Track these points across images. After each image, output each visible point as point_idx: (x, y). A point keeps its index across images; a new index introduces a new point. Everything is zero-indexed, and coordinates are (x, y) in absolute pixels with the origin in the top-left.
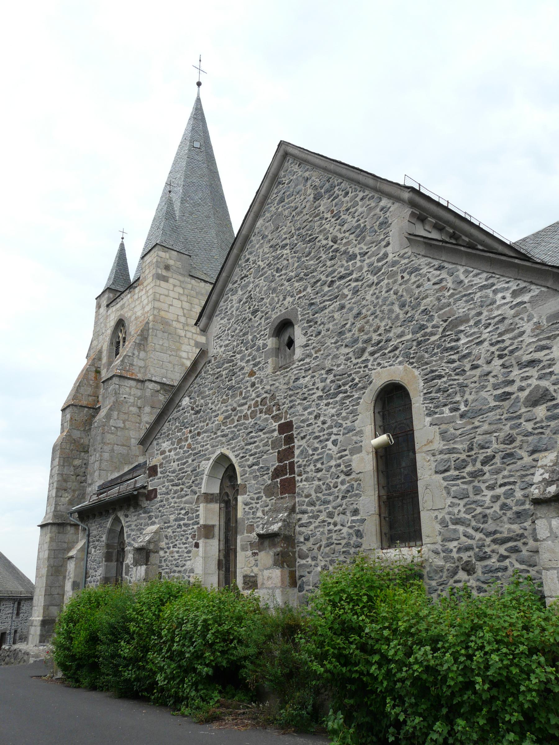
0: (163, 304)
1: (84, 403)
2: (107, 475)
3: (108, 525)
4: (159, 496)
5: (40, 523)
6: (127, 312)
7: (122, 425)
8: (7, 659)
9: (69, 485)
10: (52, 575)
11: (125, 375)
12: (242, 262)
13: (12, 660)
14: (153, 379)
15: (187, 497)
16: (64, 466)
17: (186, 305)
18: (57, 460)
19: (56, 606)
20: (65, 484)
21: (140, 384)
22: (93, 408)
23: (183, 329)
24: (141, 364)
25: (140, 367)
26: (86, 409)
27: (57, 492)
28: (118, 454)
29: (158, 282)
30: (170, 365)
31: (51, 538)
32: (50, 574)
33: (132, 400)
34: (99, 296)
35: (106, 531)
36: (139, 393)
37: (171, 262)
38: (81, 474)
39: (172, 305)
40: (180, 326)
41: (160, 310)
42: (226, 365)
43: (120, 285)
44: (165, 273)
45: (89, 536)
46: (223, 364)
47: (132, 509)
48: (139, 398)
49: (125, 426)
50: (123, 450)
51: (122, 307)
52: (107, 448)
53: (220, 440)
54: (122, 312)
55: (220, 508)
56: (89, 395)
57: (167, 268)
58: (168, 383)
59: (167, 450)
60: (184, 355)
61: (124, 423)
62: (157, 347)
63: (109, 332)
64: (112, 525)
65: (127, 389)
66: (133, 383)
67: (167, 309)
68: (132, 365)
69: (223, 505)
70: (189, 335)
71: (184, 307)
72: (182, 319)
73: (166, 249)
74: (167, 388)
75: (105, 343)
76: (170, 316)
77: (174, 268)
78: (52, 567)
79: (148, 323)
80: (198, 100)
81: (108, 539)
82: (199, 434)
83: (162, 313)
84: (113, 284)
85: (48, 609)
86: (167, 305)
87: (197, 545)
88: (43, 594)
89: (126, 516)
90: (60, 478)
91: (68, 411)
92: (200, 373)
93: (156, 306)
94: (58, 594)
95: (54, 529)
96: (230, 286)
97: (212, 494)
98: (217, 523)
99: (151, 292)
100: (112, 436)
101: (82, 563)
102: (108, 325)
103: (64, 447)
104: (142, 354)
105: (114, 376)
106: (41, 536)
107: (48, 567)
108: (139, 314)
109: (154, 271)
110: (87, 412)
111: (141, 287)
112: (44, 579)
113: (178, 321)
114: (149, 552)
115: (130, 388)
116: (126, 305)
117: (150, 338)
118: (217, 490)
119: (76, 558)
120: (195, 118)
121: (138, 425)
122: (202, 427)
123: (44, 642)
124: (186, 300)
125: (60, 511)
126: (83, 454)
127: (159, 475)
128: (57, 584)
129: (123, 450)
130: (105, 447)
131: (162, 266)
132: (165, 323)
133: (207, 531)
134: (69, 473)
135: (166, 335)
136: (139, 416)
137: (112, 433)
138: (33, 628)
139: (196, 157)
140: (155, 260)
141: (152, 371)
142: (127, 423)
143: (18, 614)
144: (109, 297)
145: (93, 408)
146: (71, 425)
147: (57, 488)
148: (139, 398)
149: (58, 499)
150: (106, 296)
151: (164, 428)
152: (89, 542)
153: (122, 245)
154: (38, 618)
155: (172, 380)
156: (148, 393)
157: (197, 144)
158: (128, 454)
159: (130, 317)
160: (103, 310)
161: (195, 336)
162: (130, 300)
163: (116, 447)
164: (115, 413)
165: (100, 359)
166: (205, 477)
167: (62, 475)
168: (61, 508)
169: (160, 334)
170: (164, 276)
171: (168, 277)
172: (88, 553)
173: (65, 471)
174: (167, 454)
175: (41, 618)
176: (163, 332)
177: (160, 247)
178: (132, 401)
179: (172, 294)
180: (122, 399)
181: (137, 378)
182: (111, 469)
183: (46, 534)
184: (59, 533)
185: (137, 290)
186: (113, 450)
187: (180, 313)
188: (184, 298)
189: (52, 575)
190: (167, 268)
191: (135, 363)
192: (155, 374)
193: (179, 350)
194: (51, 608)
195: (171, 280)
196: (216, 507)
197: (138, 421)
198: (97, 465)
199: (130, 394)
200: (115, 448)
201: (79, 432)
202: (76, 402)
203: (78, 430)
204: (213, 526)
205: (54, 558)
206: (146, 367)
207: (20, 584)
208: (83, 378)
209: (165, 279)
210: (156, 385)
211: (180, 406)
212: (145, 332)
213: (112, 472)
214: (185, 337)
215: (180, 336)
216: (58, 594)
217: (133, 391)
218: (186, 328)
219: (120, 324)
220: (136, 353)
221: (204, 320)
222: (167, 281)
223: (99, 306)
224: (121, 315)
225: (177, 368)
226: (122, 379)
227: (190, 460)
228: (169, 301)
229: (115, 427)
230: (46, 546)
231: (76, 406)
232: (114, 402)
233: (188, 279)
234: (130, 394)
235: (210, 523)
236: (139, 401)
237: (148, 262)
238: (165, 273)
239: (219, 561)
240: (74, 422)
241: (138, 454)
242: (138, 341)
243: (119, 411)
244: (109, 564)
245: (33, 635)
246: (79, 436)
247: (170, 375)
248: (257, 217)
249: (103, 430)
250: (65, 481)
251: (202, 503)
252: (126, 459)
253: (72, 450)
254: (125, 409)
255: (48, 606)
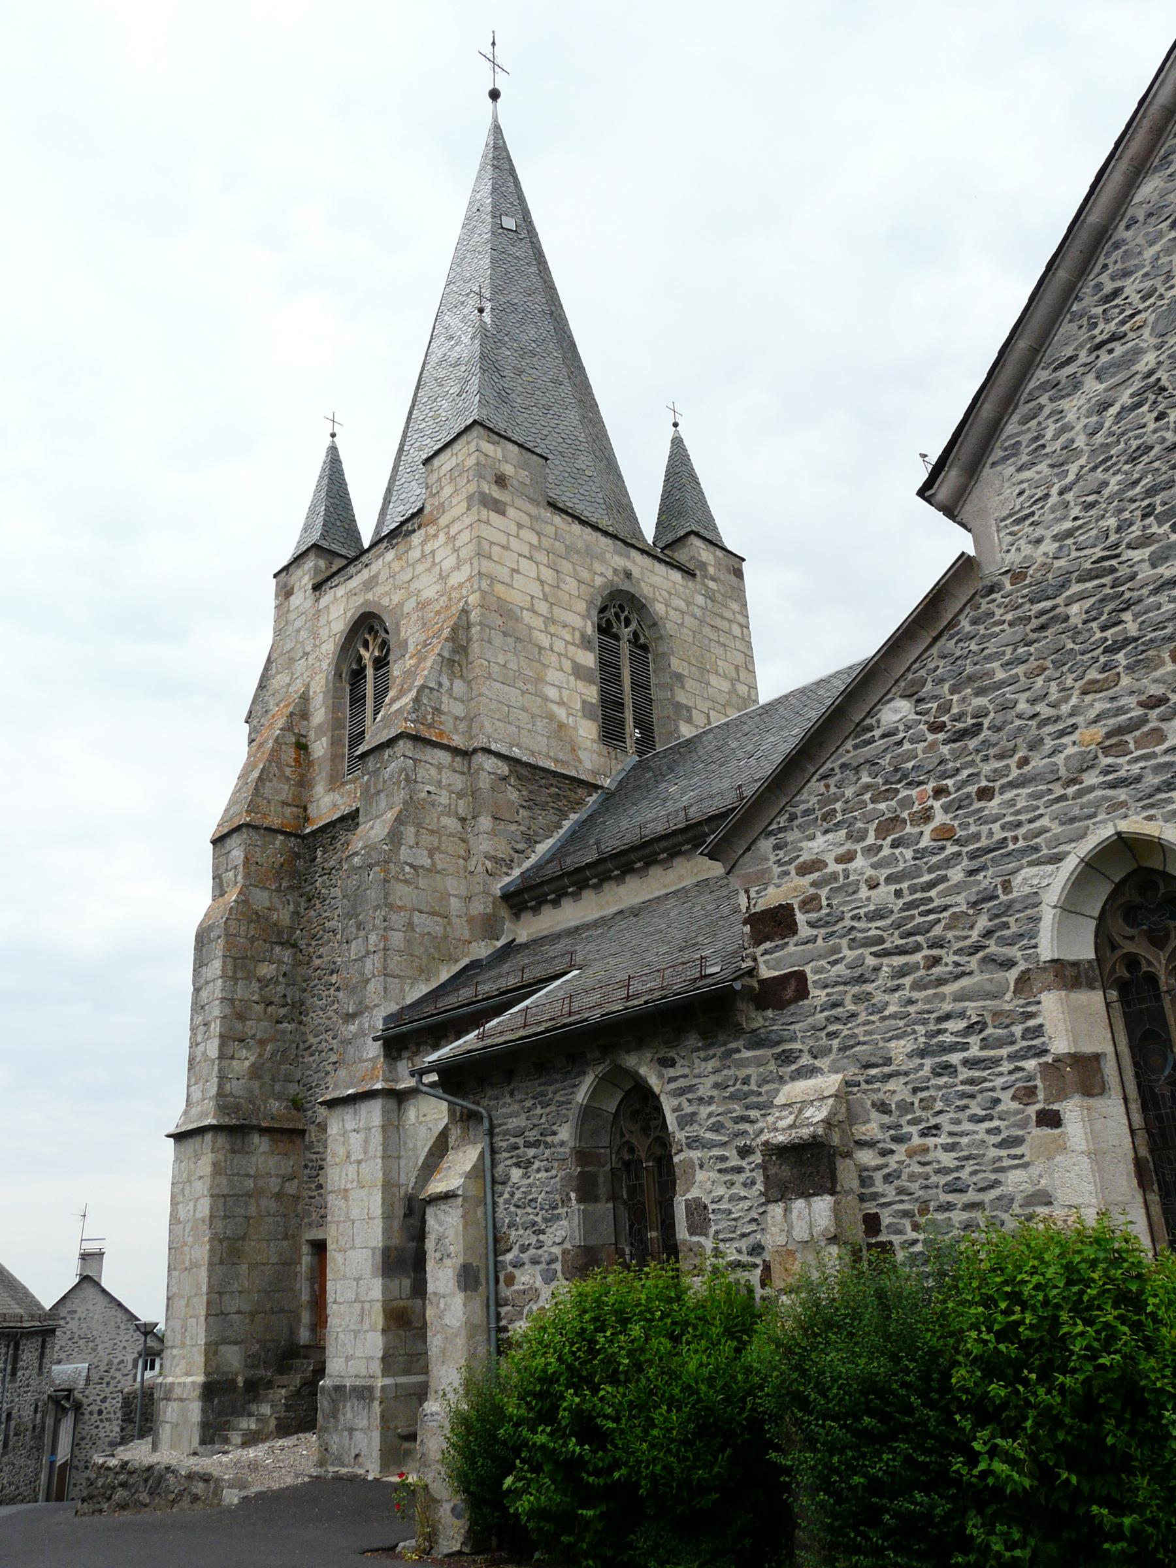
0: (499, 567)
1: (276, 822)
2: (402, 990)
3: (581, 1095)
4: (814, 992)
5: (172, 1129)
6: (387, 593)
7: (427, 862)
8: (120, 1494)
9: (251, 1027)
10: (221, 1262)
11: (427, 735)
12: (1088, 302)
13: (144, 1497)
14: (493, 747)
15: (964, 982)
16: (235, 979)
17: (548, 574)
18: (217, 964)
19: (236, 1343)
20: (239, 1026)
21: (458, 759)
22: (297, 836)
23: (546, 631)
24: (459, 710)
25: (457, 718)
26: (281, 838)
27: (222, 1047)
28: (423, 935)
29: (484, 512)
30: (524, 717)
31: (214, 1164)
32: (216, 1260)
33: (444, 799)
34: (286, 569)
35: (573, 1113)
36: (459, 782)
37: (508, 470)
38: (276, 1000)
39: (517, 571)
40: (538, 622)
41: (493, 580)
42: (1075, 588)
43: (333, 549)
44: (496, 492)
45: (491, 1133)
46: (1064, 586)
47: (693, 1041)
48: (460, 795)
49: (434, 864)
50: (433, 926)
51: (370, 584)
52: (398, 919)
53: (1105, 798)
54: (370, 596)
55: (1108, 1005)
56: (284, 804)
57: (501, 481)
58: (524, 759)
59: (830, 858)
60: (552, 693)
61: (431, 856)
62: (495, 669)
63: (329, 648)
64: (594, 1094)
65: (433, 771)
66: (443, 757)
67: (507, 580)
68: (437, 711)
69: (1114, 994)
70: (559, 646)
71: (543, 578)
72: (542, 607)
73: (496, 438)
74: (524, 772)
75: (317, 674)
76: (516, 598)
77: (516, 483)
78: (221, 1241)
79: (465, 612)
80: (497, 130)
81: (580, 1135)
82: (985, 794)
83: (499, 589)
84: (323, 537)
85: (216, 1353)
86: (506, 571)
87: (1050, 1119)
88: (203, 1312)
89: (669, 1063)
90: (228, 1011)
91: (235, 840)
92: (951, 625)
93: (483, 570)
94: (238, 1312)
95: (222, 1140)
96: (1042, 375)
97: (1075, 964)
98: (1109, 1049)
99: (465, 537)
100: (406, 889)
101: (480, 1212)
102: (324, 633)
103: (232, 931)
104: (459, 687)
105: (400, 736)
106: (178, 1160)
107: (211, 1240)
108: (430, 593)
109: (472, 488)
110: (283, 843)
111: (431, 530)
112: (203, 1273)
113: (532, 610)
114: (834, 1156)
115: (440, 768)
116: (383, 577)
117: (475, 648)
118: (1085, 951)
119: (465, 1199)
120: (495, 167)
121: (461, 862)
122: (997, 774)
123: (212, 1442)
124: (545, 562)
125: (231, 1095)
126: (278, 949)
127: (804, 931)
128: (236, 1287)
129: (433, 926)
130: (394, 917)
131: (490, 477)
132: (506, 612)
133: (1083, 1073)
134: (247, 996)
135: (511, 641)
136: (463, 840)
137: (405, 881)
138: (173, 1405)
139: (512, 250)
140: (471, 461)
141: (489, 729)
142: (437, 856)
143: (14, 1373)
144: (316, 569)
145: (297, 836)
146: (247, 876)
147: (221, 1036)
148: (460, 795)
149: (225, 1063)
150: (310, 563)
151: (804, 796)
152: (493, 1151)
153: (333, 452)
154: (190, 1379)
155: (533, 753)
156: (484, 782)
157: (509, 223)
158: (446, 937)
159: (401, 605)
160: (301, 599)
161: (572, 649)
162: (396, 566)
163: (417, 918)
164: (410, 831)
165: (305, 715)
166: (1048, 915)
167: (232, 1001)
168: (235, 1087)
169: (498, 639)
170: (496, 501)
171: (506, 504)
172: (494, 1182)
173: (241, 992)
174: (833, 867)
175: (200, 1379)
176: (505, 634)
177: (480, 429)
178: (444, 800)
179: (515, 544)
180: (424, 795)
181: (453, 744)
182: (410, 973)
183: (197, 1157)
184: (233, 1151)
185: (416, 539)
186: (410, 926)
187: (536, 590)
188: (542, 557)
189: (221, 1262)
190: (501, 481)
191: (444, 708)
192: (496, 736)
193: (540, 680)
194: (223, 1349)
195: (511, 512)
196: (1094, 1000)
197: (462, 853)
198: (372, 965)
199: (439, 784)
200: (416, 920)
201: (266, 894)
202: (257, 819)
203: (264, 888)
204: (1097, 1057)
205: (226, 1217)
206: (470, 719)
207: (13, 1298)
208: (270, 761)
209: (499, 508)
210: (500, 764)
211: (870, 729)
212: (461, 634)
213: (415, 980)
214: (552, 649)
215: (541, 648)
216: (238, 1312)
217: (447, 777)
218: (552, 629)
219: (367, 625)
220: (446, 683)
221: (951, 478)
222: (503, 514)
223: (285, 593)
224: (366, 602)
225: (540, 724)
226: (419, 745)
227: (956, 875)
228: (510, 559)
229: (411, 866)
230: (201, 1188)
231: (256, 828)
232: (405, 803)
233: (547, 514)
234: (439, 784)
235: (1089, 1048)
236: (461, 802)
237: (446, 468)
238: (496, 492)
239: (1138, 1163)
240: (253, 868)
241: (467, 937)
242: (446, 654)
243: (419, 826)
244: (591, 1207)
245: (175, 1426)
246: (267, 904)
247: (526, 740)
248: (1139, 172)
249: (387, 871)
250: (241, 1017)
251: (1049, 988)
252: (442, 950)
253: (252, 940)
254: (431, 819)
255: (217, 1344)
